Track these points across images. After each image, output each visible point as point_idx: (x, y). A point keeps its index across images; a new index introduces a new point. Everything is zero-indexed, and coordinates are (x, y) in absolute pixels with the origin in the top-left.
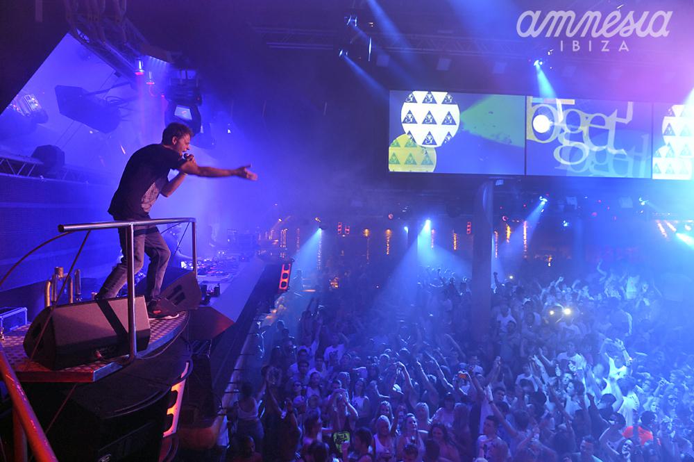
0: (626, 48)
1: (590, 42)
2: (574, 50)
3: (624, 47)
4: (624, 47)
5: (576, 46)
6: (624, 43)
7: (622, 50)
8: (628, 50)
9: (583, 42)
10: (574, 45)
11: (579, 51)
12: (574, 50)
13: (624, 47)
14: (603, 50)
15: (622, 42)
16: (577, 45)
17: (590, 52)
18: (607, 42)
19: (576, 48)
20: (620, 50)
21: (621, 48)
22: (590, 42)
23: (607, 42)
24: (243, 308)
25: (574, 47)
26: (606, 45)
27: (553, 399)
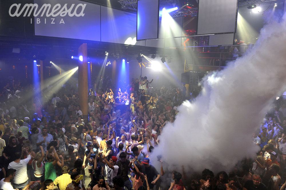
0: (63, 22)
2: (37, 23)
4: (62, 21)
6: (62, 20)
8: (64, 23)
10: (37, 21)
12: (37, 23)
16: (39, 21)
18: (54, 19)
19: (38, 22)
21: (61, 22)
23: (54, 19)
25: (37, 22)
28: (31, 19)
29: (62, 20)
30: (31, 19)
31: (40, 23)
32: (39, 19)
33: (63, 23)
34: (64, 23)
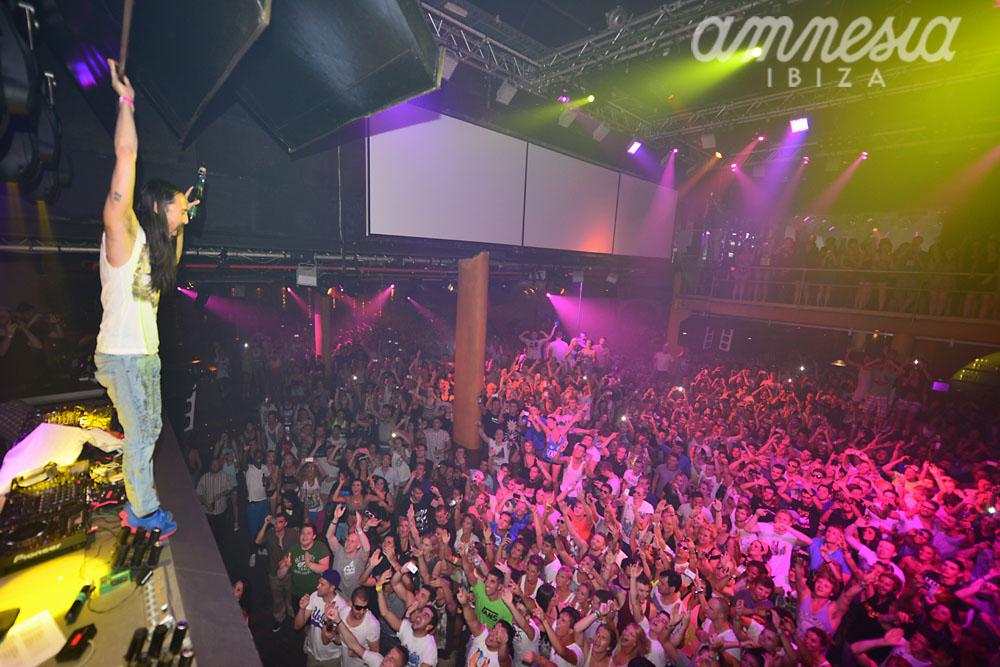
0: (881, 81)
1: (819, 70)
4: (876, 78)
5: (794, 77)
6: (877, 72)
7: (873, 85)
9: (808, 71)
10: (791, 76)
11: (801, 85)
12: (791, 84)
14: (842, 84)
15: (873, 71)
16: (796, 76)
17: (853, 85)
18: (848, 71)
20: (870, 85)
21: (872, 81)
22: (819, 70)
23: (848, 71)
24: (104, 314)
26: (846, 75)
27: (500, 575)
28: (770, 71)
30: (770, 71)
32: (798, 71)
33: (880, 85)
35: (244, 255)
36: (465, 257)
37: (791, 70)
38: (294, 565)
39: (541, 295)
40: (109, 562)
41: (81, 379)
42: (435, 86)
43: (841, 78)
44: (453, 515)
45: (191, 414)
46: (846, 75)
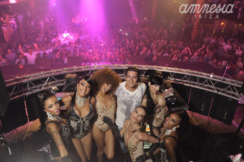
0: (218, 17)
3: (217, 17)
4: (217, 17)
6: (217, 15)
7: (216, 18)
8: (218, 18)
10: (200, 16)
12: (200, 18)
13: (217, 17)
14: (210, 18)
16: (201, 16)
18: (211, 15)
19: (200, 17)
21: (216, 17)
23: (211, 15)
26: (211, 16)
29: (217, 15)
31: (201, 18)
32: (201, 15)
33: (218, 18)
34: (218, 18)
35: (51, 79)
36: (40, 120)
37: (200, 15)
38: (187, 110)
39: (204, 44)
40: (63, 145)
41: (25, 101)
42: (181, 112)
43: (211, 16)
44: (53, 72)
45: (28, 118)
46: (211, 16)
